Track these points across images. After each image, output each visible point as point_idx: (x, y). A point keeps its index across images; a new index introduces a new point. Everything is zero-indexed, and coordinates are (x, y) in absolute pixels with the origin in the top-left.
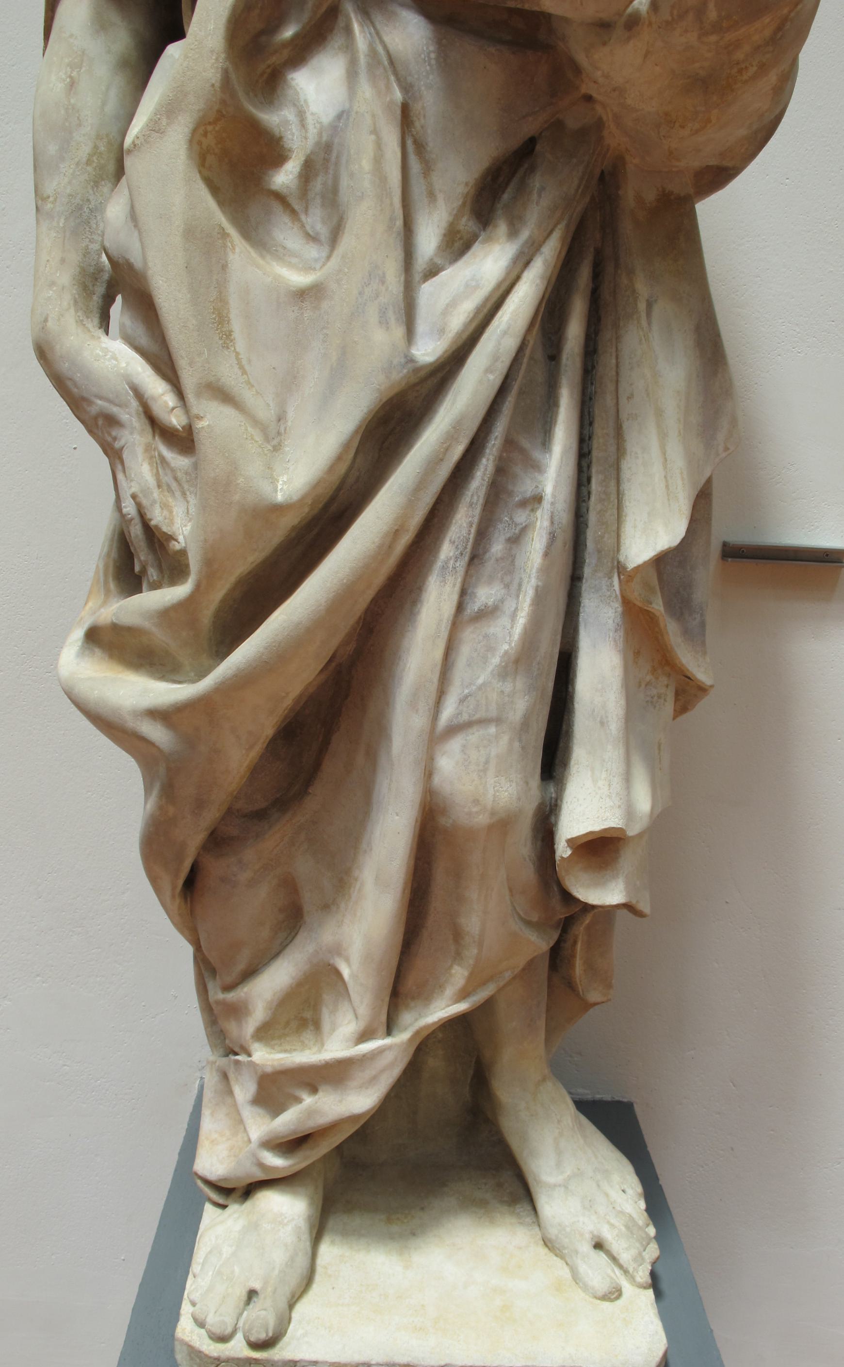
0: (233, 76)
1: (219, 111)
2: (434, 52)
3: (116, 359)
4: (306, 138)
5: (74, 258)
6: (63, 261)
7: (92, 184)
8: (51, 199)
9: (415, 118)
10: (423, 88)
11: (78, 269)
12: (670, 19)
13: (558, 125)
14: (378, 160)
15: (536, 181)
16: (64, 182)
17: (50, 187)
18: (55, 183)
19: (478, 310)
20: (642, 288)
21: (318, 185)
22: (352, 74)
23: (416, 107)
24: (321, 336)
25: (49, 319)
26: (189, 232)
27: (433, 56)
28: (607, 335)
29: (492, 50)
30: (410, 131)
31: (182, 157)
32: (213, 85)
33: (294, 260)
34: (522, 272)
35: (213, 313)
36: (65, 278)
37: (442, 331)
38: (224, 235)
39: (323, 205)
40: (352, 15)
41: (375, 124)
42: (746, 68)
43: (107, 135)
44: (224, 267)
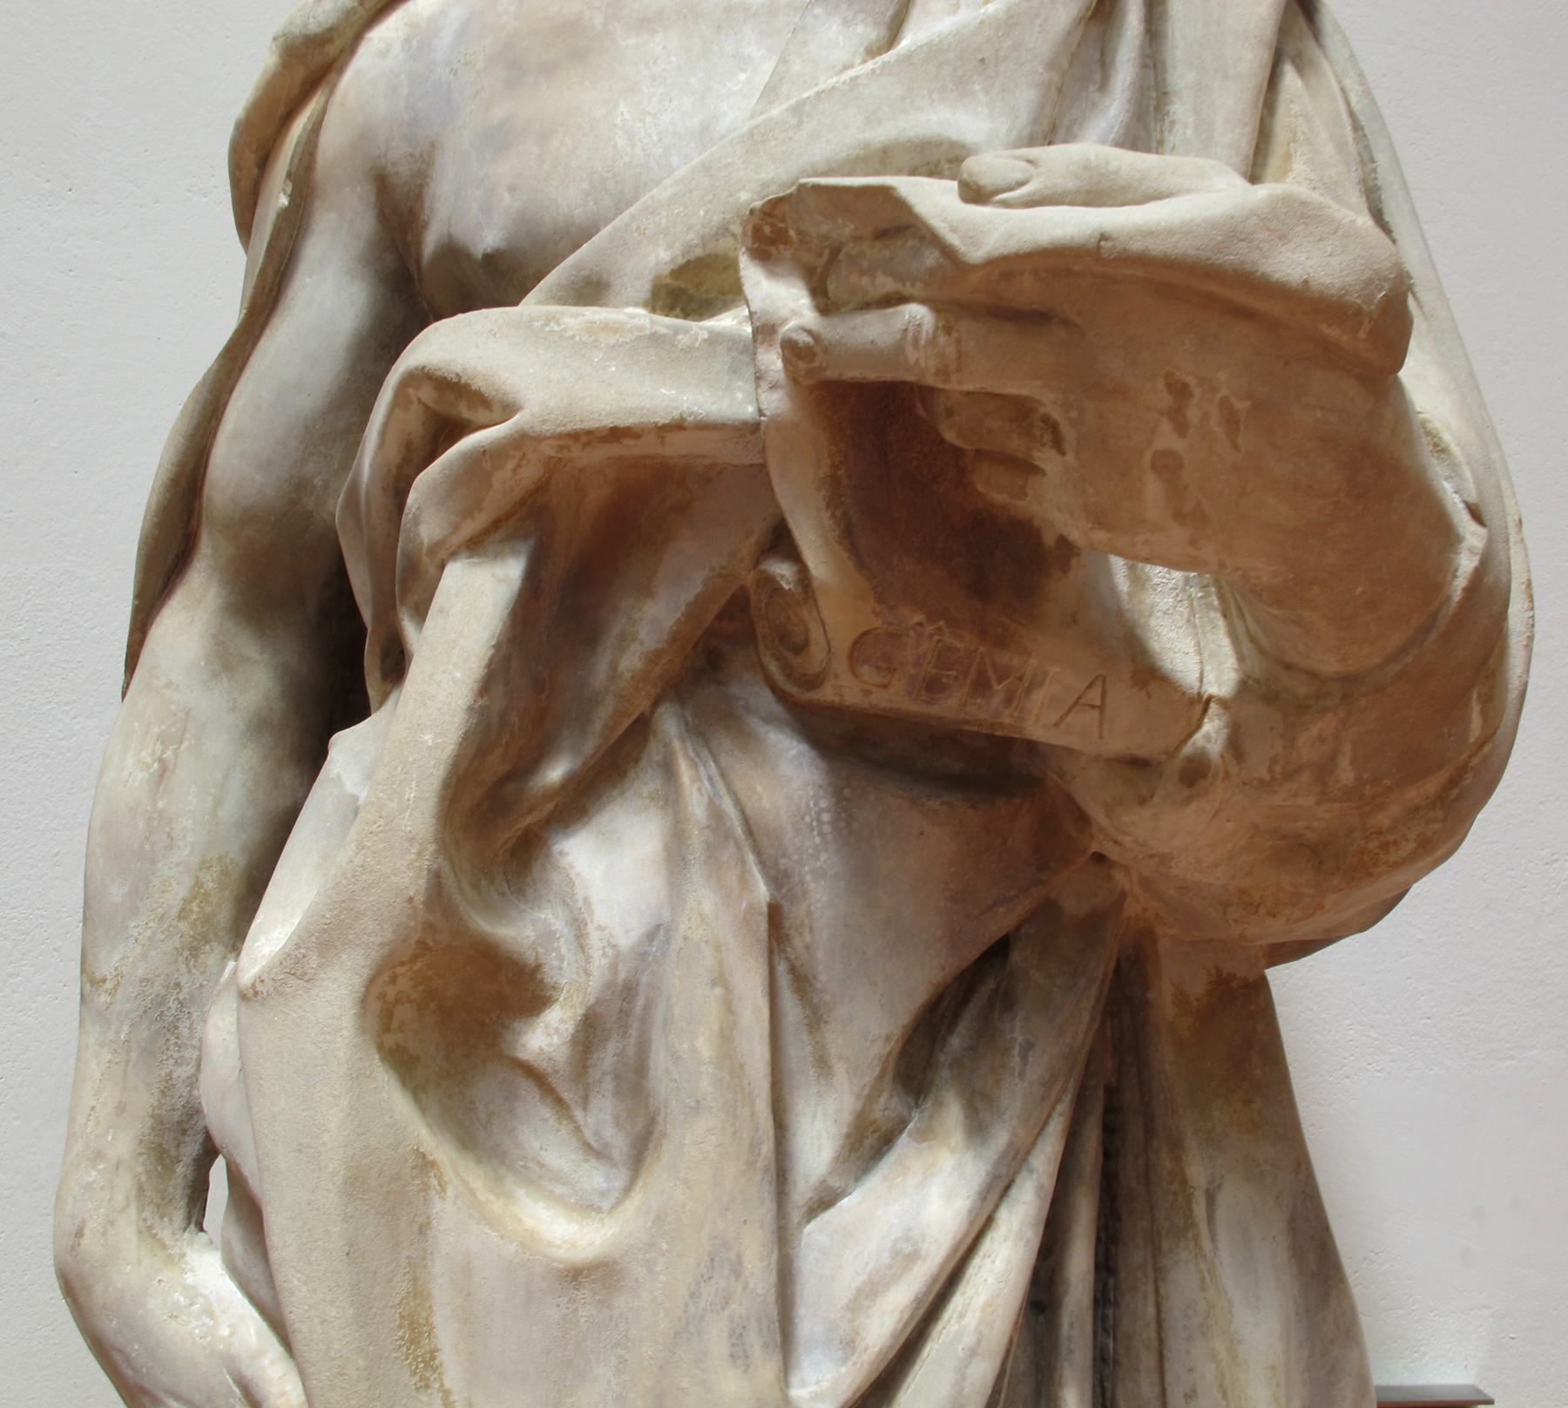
0: (449, 879)
1: (421, 943)
2: (828, 811)
3: (211, 1315)
4: (587, 974)
5: (144, 1101)
6: (121, 1109)
7: (186, 953)
8: (108, 985)
9: (793, 932)
10: (808, 878)
11: (150, 1122)
12: (1267, 777)
13: (1048, 911)
14: (727, 1037)
15: (1016, 1030)
16: (132, 956)
17: (109, 963)
18: (117, 957)
19: (918, 1301)
20: (1197, 1172)
21: (607, 1057)
22: (675, 857)
23: (795, 914)
24: (613, 1360)
25: (87, 1231)
26: (355, 1182)
27: (826, 817)
28: (1134, 1255)
29: (934, 804)
30: (784, 951)
31: (345, 1033)
32: (411, 900)
33: (560, 1190)
34: (996, 1207)
35: (400, 1327)
36: (124, 1143)
37: (849, 1345)
38: (425, 1165)
39: (616, 1093)
40: (677, 744)
41: (720, 964)
42: (1395, 842)
43: (220, 859)
44: (423, 1229)
